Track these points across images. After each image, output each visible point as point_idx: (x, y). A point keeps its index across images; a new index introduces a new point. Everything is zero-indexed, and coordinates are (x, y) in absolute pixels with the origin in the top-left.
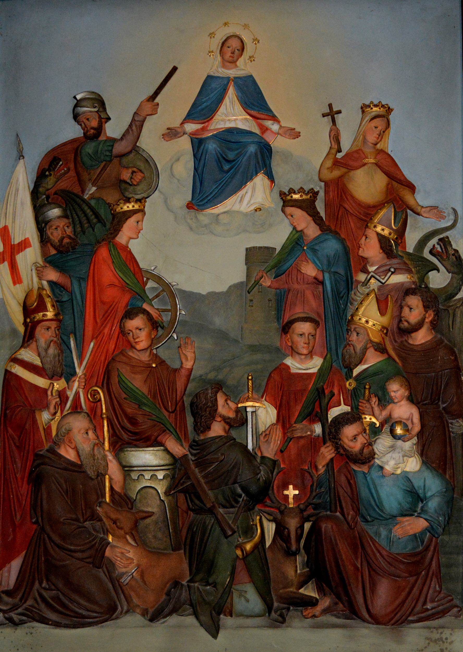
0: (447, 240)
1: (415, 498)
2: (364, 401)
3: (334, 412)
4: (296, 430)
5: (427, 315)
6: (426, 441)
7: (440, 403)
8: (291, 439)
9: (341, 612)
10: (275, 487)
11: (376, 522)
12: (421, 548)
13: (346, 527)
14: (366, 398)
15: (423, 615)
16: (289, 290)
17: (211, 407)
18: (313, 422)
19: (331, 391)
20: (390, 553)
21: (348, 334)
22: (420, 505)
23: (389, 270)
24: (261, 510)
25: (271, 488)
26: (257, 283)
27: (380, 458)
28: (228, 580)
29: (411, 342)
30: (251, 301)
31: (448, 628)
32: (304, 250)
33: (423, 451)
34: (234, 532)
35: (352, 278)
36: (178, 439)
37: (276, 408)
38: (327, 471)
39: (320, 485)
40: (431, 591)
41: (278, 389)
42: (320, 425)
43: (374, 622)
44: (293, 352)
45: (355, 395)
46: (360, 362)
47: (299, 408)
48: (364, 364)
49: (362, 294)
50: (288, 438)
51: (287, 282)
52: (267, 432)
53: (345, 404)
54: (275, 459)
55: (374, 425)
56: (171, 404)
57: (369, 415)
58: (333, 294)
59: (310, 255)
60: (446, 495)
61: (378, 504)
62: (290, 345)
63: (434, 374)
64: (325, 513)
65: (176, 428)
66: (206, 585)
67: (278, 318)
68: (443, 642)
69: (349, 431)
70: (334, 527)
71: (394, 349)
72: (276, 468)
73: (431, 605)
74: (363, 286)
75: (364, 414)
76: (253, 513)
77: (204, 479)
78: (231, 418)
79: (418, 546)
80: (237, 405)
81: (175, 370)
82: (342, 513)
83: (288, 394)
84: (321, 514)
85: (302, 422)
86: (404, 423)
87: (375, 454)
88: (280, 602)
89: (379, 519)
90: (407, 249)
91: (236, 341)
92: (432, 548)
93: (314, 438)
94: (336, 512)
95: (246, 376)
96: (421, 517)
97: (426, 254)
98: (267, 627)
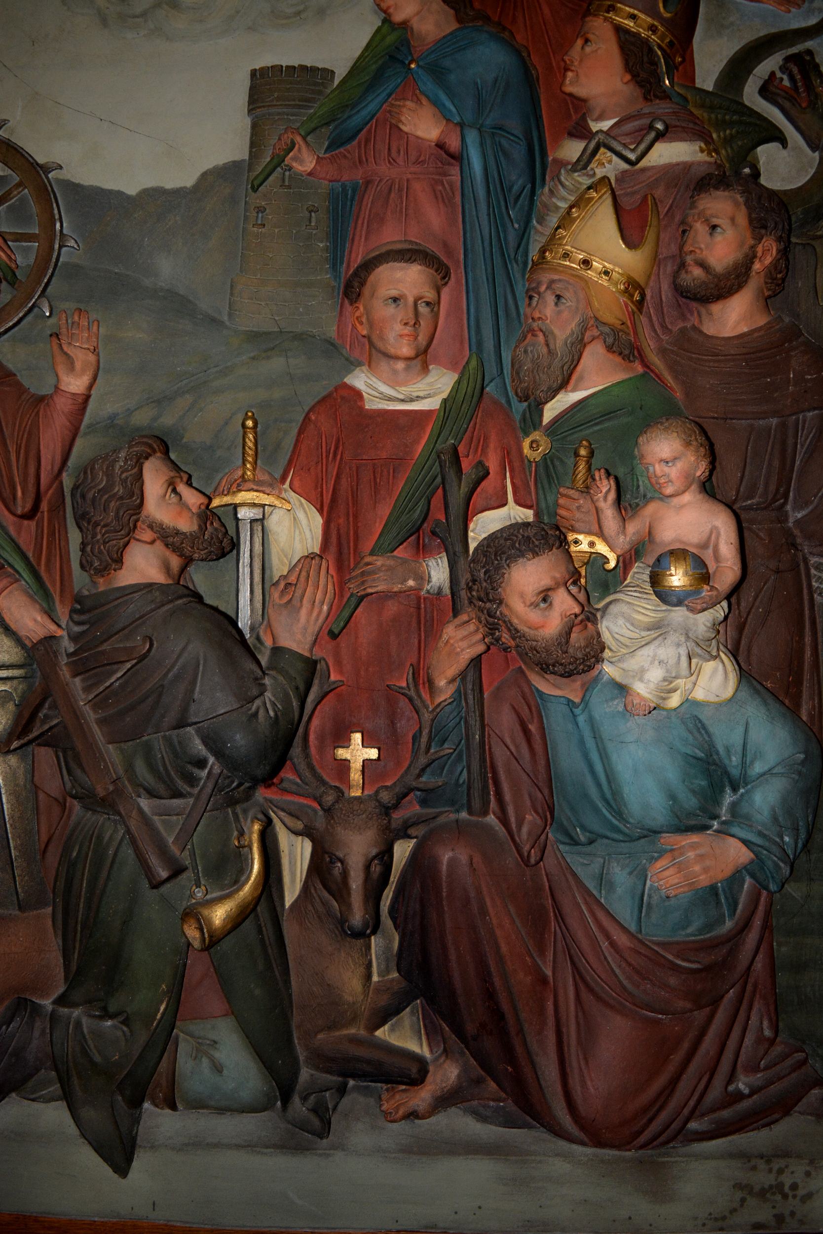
0: (808, 58)
1: (713, 778)
2: (571, 492)
3: (486, 524)
4: (374, 572)
5: (760, 249)
6: (749, 613)
7: (789, 507)
8: (361, 599)
9: (492, 1103)
10: (312, 737)
11: (599, 847)
12: (729, 924)
13: (511, 859)
14: (580, 484)
15: (726, 1114)
16: (368, 183)
17: (121, 498)
18: (422, 550)
19: (480, 463)
20: (640, 941)
21: (530, 305)
22: (728, 798)
23: (651, 127)
24: (271, 802)
25: (298, 740)
26: (278, 161)
27: (619, 660)
28: (162, 1008)
29: (709, 329)
30: (261, 210)
31: (799, 1156)
32: (410, 69)
33: (737, 641)
34: (177, 871)
35: (544, 153)
36: (43, 596)
37: (320, 511)
38: (459, 695)
39: (438, 735)
40: (748, 1041)
41: (327, 457)
42: (445, 559)
43: (586, 1139)
44: (373, 351)
45: (548, 476)
46: (564, 385)
47: (384, 511)
48: (574, 390)
49: (570, 192)
50: (352, 594)
51: (360, 162)
52: (292, 579)
53: (518, 502)
54: (317, 654)
55: (600, 562)
56: (23, 493)
57: (589, 533)
58: (488, 187)
59: (427, 84)
60: (804, 770)
61: (608, 795)
62: (365, 332)
63: (774, 421)
64: (453, 816)
65: (39, 564)
66: (101, 1018)
67: (335, 259)
68: (785, 1196)
69: (527, 577)
70: (477, 859)
71: (663, 352)
72: (316, 682)
73: (746, 1080)
74: (575, 171)
75: (574, 530)
76: (245, 811)
77: (95, 712)
78: (184, 534)
79: (721, 920)
80: (210, 500)
81: (41, 399)
82: (504, 820)
83: (354, 469)
84: (442, 819)
85: (392, 552)
86: (694, 555)
87: (603, 649)
88: (317, 1068)
89: (607, 838)
90: (697, 81)
91: (214, 322)
92: (757, 922)
93: (425, 599)
94: (485, 813)
95: (240, 417)
96: (733, 836)
97: (751, 95)
98: (275, 1146)
